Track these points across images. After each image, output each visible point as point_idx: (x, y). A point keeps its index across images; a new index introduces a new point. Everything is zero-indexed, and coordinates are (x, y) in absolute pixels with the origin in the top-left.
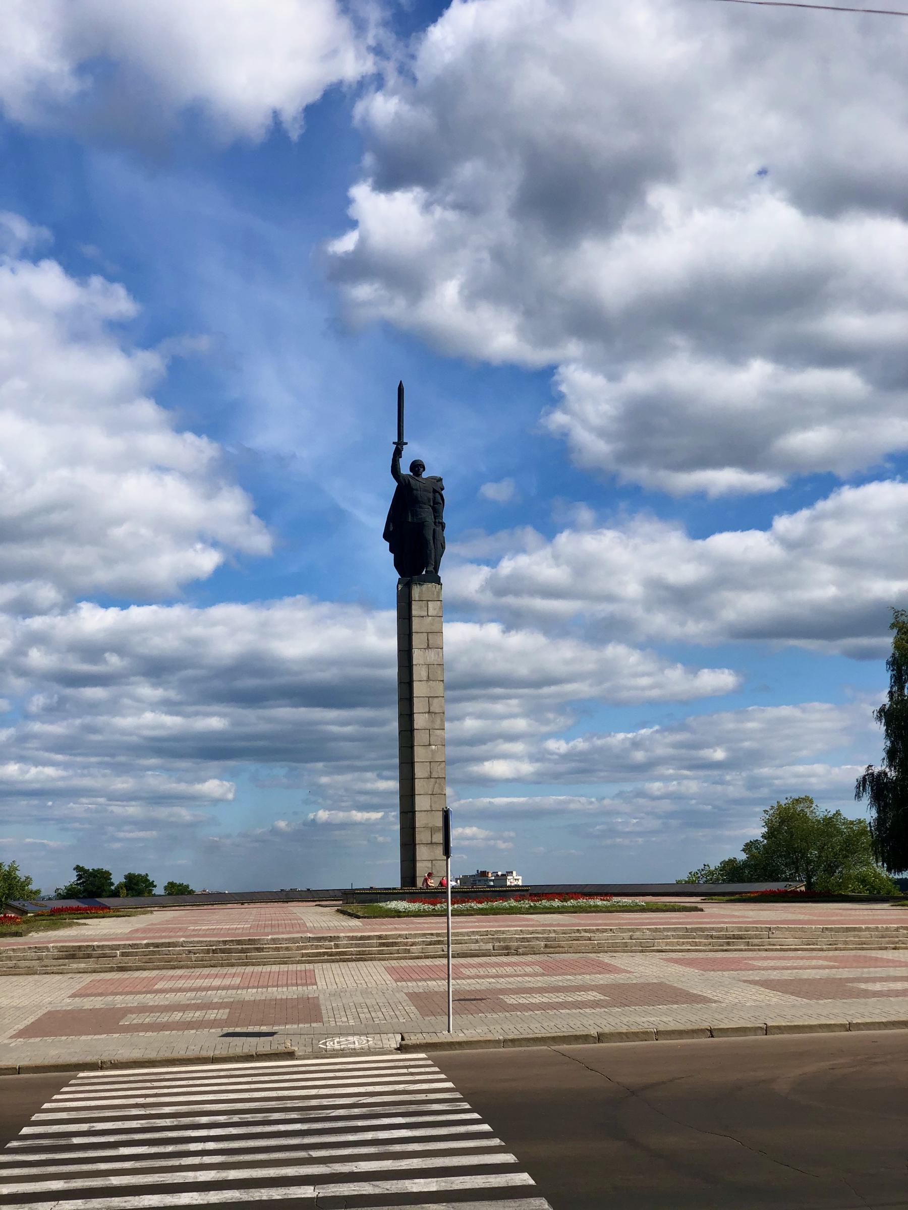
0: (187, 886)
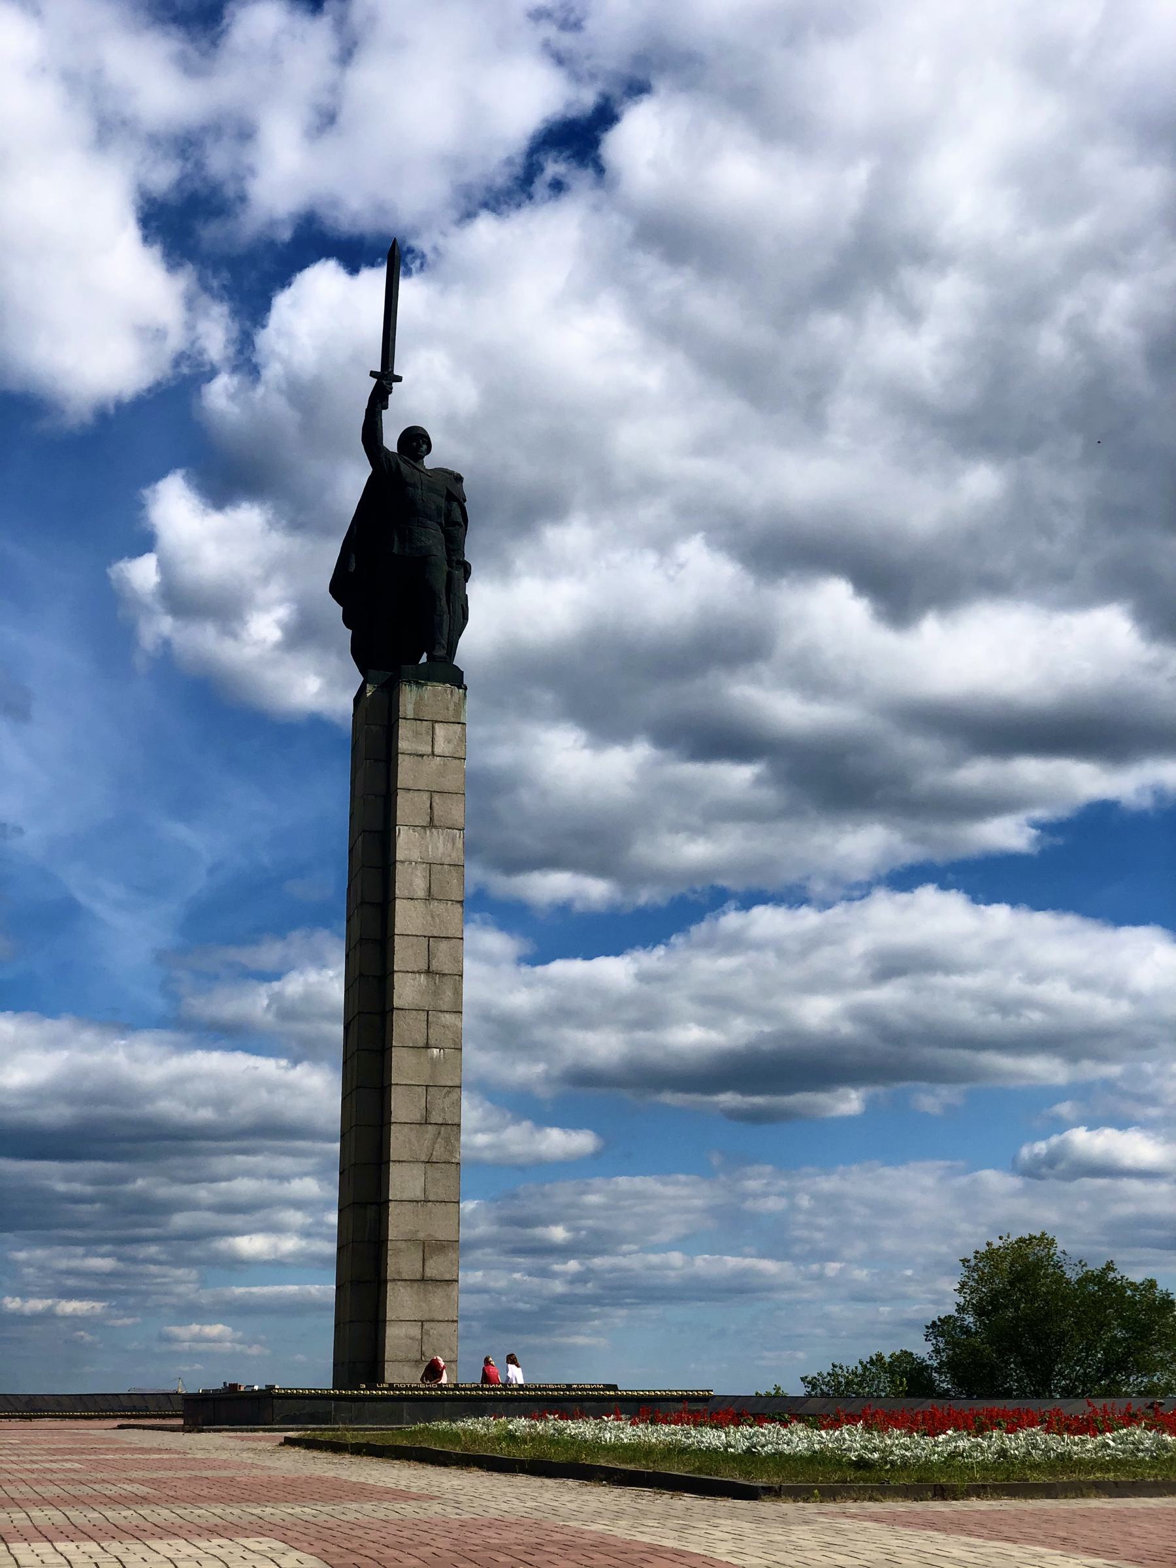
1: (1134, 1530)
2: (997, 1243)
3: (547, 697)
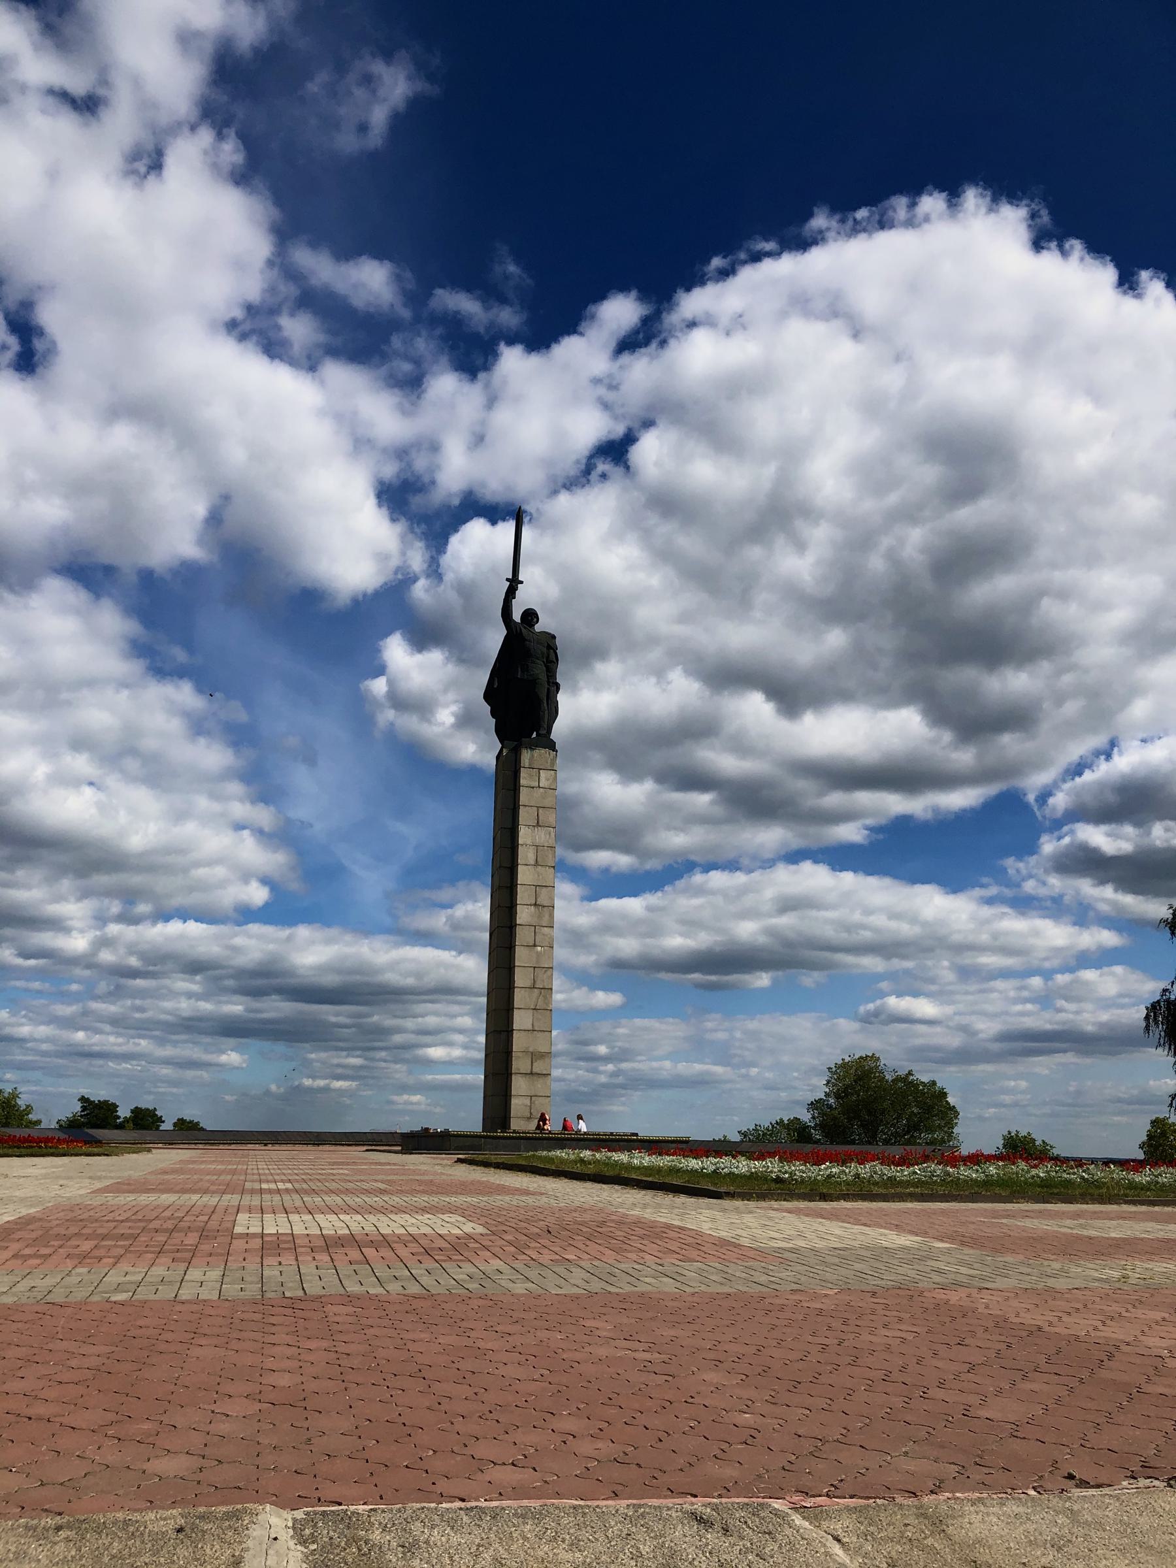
0: (198, 1124)
1: (937, 1222)
2: (847, 1059)
3: (598, 757)
